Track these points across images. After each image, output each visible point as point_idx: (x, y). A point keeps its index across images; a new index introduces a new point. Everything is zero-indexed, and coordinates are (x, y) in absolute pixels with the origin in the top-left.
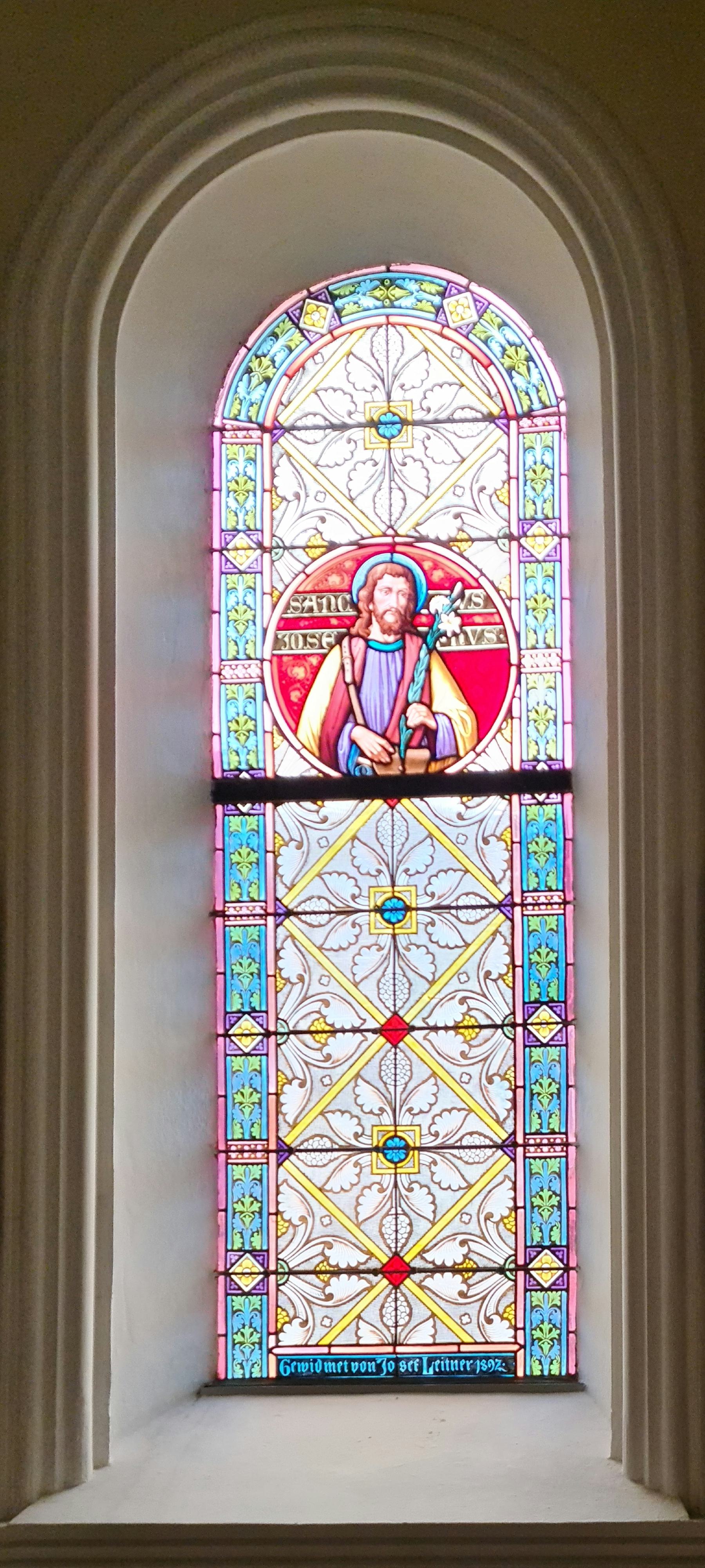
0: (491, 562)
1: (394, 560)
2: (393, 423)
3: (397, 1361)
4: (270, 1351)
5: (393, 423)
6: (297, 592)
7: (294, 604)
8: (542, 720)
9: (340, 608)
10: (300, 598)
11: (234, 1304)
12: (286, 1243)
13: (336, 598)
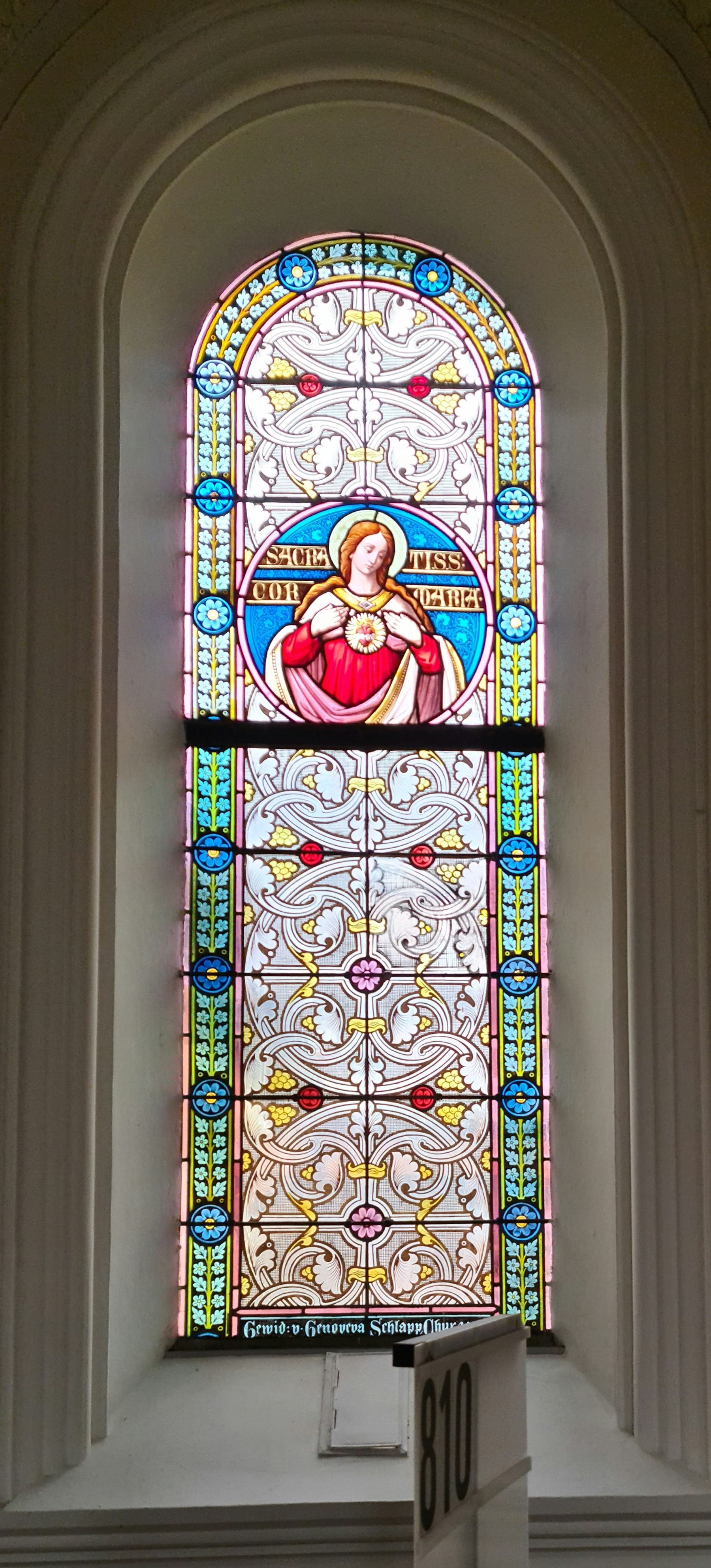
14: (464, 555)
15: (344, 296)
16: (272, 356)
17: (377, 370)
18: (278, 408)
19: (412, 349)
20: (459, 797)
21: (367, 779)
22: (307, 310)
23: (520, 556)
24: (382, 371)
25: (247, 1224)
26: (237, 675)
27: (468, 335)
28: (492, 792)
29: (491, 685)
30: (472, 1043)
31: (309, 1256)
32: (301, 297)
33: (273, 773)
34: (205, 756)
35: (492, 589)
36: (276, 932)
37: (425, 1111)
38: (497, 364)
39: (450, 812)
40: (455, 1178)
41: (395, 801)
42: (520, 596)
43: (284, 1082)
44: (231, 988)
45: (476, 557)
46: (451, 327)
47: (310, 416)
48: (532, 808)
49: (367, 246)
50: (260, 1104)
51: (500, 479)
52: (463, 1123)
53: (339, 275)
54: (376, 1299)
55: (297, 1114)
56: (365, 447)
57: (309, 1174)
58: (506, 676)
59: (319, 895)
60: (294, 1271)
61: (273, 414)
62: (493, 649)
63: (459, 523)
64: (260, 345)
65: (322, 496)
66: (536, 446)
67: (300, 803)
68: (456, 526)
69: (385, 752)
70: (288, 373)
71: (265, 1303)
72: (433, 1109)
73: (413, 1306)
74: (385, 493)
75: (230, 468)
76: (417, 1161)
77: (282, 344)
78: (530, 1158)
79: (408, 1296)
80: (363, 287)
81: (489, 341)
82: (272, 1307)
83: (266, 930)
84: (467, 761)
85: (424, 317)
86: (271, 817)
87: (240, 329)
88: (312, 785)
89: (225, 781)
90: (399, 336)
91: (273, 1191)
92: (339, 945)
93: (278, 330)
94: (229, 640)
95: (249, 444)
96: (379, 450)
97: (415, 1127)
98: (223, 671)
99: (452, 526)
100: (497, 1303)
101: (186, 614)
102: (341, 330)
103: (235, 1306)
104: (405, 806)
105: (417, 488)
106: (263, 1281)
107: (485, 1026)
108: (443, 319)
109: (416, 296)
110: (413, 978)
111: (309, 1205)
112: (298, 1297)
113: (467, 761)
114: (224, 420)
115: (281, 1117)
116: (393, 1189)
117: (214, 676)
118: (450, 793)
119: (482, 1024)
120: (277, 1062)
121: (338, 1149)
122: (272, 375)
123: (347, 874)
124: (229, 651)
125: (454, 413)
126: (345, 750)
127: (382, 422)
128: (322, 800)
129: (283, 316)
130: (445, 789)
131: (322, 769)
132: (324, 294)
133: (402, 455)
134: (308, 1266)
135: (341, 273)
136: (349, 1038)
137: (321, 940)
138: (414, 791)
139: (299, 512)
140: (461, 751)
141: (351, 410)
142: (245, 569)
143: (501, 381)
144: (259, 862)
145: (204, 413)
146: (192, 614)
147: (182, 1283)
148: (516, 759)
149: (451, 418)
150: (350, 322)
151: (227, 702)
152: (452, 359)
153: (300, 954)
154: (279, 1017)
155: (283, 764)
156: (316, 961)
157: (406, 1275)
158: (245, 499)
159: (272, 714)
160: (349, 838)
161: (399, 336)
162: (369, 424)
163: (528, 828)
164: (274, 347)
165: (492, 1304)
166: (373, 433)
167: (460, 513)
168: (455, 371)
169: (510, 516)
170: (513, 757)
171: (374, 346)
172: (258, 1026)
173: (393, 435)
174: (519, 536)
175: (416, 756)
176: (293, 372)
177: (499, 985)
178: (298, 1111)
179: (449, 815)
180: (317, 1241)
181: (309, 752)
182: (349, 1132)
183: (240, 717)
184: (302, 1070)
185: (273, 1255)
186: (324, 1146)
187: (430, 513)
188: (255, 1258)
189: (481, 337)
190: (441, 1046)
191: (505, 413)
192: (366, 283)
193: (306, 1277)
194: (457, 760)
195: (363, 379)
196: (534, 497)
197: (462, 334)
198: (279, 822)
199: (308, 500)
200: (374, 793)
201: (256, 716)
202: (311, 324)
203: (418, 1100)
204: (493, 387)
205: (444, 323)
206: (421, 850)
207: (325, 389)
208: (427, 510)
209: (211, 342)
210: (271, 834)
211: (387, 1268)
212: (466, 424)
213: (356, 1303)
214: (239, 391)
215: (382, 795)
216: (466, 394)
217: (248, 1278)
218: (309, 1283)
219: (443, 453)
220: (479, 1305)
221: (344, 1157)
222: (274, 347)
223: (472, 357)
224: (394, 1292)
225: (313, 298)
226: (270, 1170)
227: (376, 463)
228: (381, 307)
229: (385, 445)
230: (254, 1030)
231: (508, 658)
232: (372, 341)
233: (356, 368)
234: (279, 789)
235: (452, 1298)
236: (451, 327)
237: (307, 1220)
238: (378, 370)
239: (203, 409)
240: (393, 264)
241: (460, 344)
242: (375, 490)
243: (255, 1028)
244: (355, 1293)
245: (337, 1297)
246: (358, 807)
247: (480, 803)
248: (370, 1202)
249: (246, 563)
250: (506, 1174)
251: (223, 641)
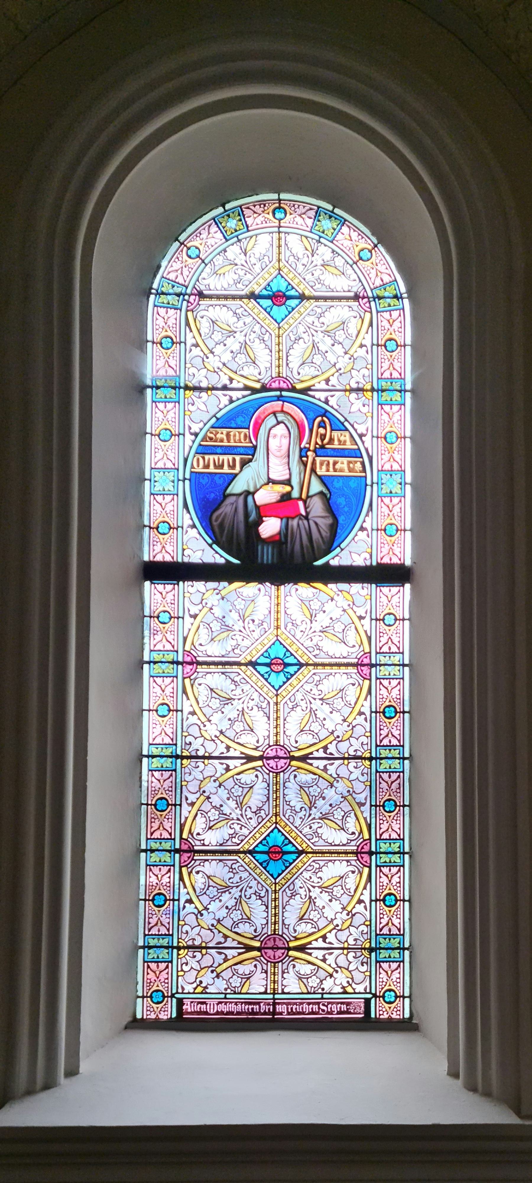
0: (356, 410)
1: (285, 409)
3: (274, 1004)
6: (213, 427)
7: (209, 434)
8: (388, 526)
9: (242, 440)
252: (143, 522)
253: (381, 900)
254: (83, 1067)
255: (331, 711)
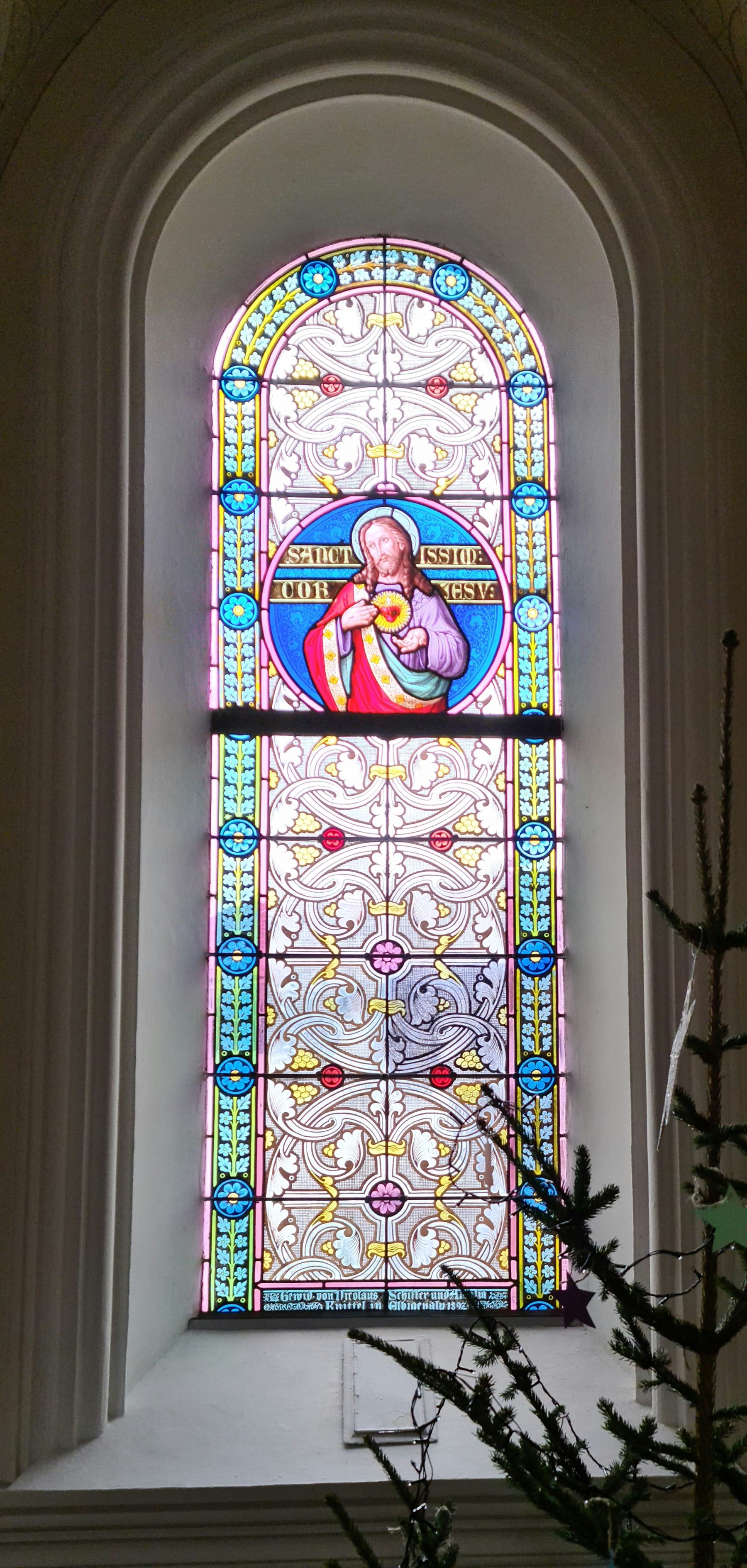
2: (393, 956)
4: (255, 1285)
5: (393, 956)
9: (331, 560)
10: (297, 548)
11: (221, 1102)
12: (282, 576)
13: (328, 550)
14: (483, 550)
15: (367, 300)
16: (297, 357)
17: (396, 369)
18: (301, 406)
19: (430, 349)
20: (478, 783)
21: (388, 766)
22: (331, 313)
23: (534, 545)
24: (402, 370)
25: (269, 1199)
26: (261, 667)
27: (485, 338)
28: (510, 778)
29: (509, 673)
30: (490, 1267)
31: (330, 1231)
32: (326, 301)
33: (297, 761)
34: (231, 745)
35: (509, 581)
36: (299, 915)
37: (442, 1089)
38: (512, 365)
39: (469, 798)
40: (472, 916)
41: (415, 787)
42: (535, 475)
43: (307, 1061)
44: (254, 1089)
45: (494, 550)
46: (468, 328)
47: (332, 414)
48: (549, 794)
49: (388, 253)
50: (282, 1083)
51: (516, 475)
52: (480, 864)
53: (359, 281)
54: (395, 1273)
55: (318, 1093)
56: (388, 780)
57: (331, 1152)
58: (525, 778)
59: (339, 1118)
60: (315, 1246)
61: (296, 412)
62: (511, 639)
63: (477, 518)
64: (286, 347)
65: (344, 491)
66: (549, 444)
67: (323, 790)
68: (474, 521)
69: (407, 739)
70: (312, 374)
71: (287, 1277)
72: (451, 1088)
73: (430, 1280)
74: (404, 488)
75: (254, 469)
76: (435, 900)
77: (307, 346)
78: (545, 1013)
79: (426, 1271)
80: (385, 292)
81: (505, 343)
82: (294, 1282)
83: (289, 913)
84: (485, 748)
85: (443, 318)
86: (295, 804)
87: (264, 335)
88: (335, 773)
89: (249, 886)
90: (419, 336)
91: (295, 1168)
92: (360, 927)
93: (302, 334)
94: (253, 862)
95: (269, 1139)
96: (399, 447)
97: (433, 1105)
98: (249, 665)
99: (471, 520)
100: (514, 1277)
101: (213, 608)
102: (364, 333)
103: (257, 1279)
104: (425, 792)
105: (436, 483)
106: (284, 1255)
107: (501, 773)
108: (462, 321)
109: (436, 300)
110: (432, 1201)
111: (332, 940)
112: (319, 1271)
113: (485, 748)
114: (248, 422)
115: (303, 1095)
116: (413, 1166)
117: (240, 668)
118: (468, 780)
119: (500, 1248)
120: (300, 1041)
121: (358, 1127)
122: (296, 376)
123: (368, 859)
124: (253, 645)
125: (472, 412)
126: (365, 737)
127: (404, 419)
128: (344, 787)
129: (308, 318)
130: (464, 775)
131: (344, 757)
132: (348, 299)
133: (422, 452)
134: (328, 1241)
135: (362, 279)
136: (369, 1262)
137: (341, 1164)
138: (434, 777)
139: (323, 506)
140: (480, 738)
141: (371, 408)
142: (269, 561)
143: (516, 380)
144: (280, 1086)
145: (229, 416)
146: (218, 609)
147: (209, 1133)
148: (534, 746)
149: (469, 416)
150: (372, 326)
151: (252, 636)
152: (470, 359)
153: (322, 937)
154: (302, 998)
155: (306, 753)
156: (339, 943)
157: (424, 773)
158: (269, 495)
159: (295, 704)
160: (370, 823)
161: (419, 336)
162: (389, 423)
163: (544, 813)
164: (299, 348)
165: (510, 1280)
166: (394, 430)
167: (478, 508)
168: (472, 371)
169: (526, 511)
170: (531, 744)
171: (395, 346)
172: (284, 771)
173: (413, 433)
174: (533, 418)
175: (436, 743)
176: (316, 373)
177: (517, 966)
178: (321, 852)
179: (468, 801)
180: (340, 974)
181: (332, 739)
182: (369, 1110)
183: (265, 707)
184: (324, 1050)
185: (297, 986)
186: (347, 884)
187: (450, 508)
188: (277, 1233)
189: (498, 339)
190: (460, 1026)
191: (519, 412)
192: (388, 288)
193: (327, 1252)
194: (476, 748)
195: (386, 380)
196: (554, 832)
197: (480, 336)
198: (302, 808)
199: (330, 495)
200: (395, 780)
201: (281, 706)
202: (335, 327)
203: (437, 842)
204: (508, 386)
205: (462, 325)
206: (440, 834)
207: (346, 388)
208: (447, 505)
209: (236, 347)
210: (295, 820)
211: (406, 1242)
212: (484, 423)
213: (376, 1278)
214: (264, 390)
215: (402, 782)
216: (488, 847)
217: (270, 1252)
218: (332, 1013)
219: (462, 450)
220: (496, 1280)
221: (365, 1134)
222: (299, 348)
223: (488, 356)
224: (413, 1266)
225: (337, 302)
226: (293, 1147)
227: (397, 460)
228: (401, 308)
229: (406, 441)
230: (277, 1010)
231: (526, 760)
232: (393, 341)
233: (377, 369)
234: (303, 776)
235: (470, 1272)
236: (468, 328)
237: (328, 1196)
238: (398, 369)
239: (228, 526)
240: (413, 270)
241: (478, 345)
242: (395, 485)
243: (279, 1009)
244: (375, 1268)
245: (357, 1271)
246: (379, 794)
247: (498, 789)
248: (390, 1178)
249: (270, 555)
250: (520, 909)
251: (248, 636)
252: (208, 703)
253: (446, 679)
254: (130, 1402)
255: (463, 904)
